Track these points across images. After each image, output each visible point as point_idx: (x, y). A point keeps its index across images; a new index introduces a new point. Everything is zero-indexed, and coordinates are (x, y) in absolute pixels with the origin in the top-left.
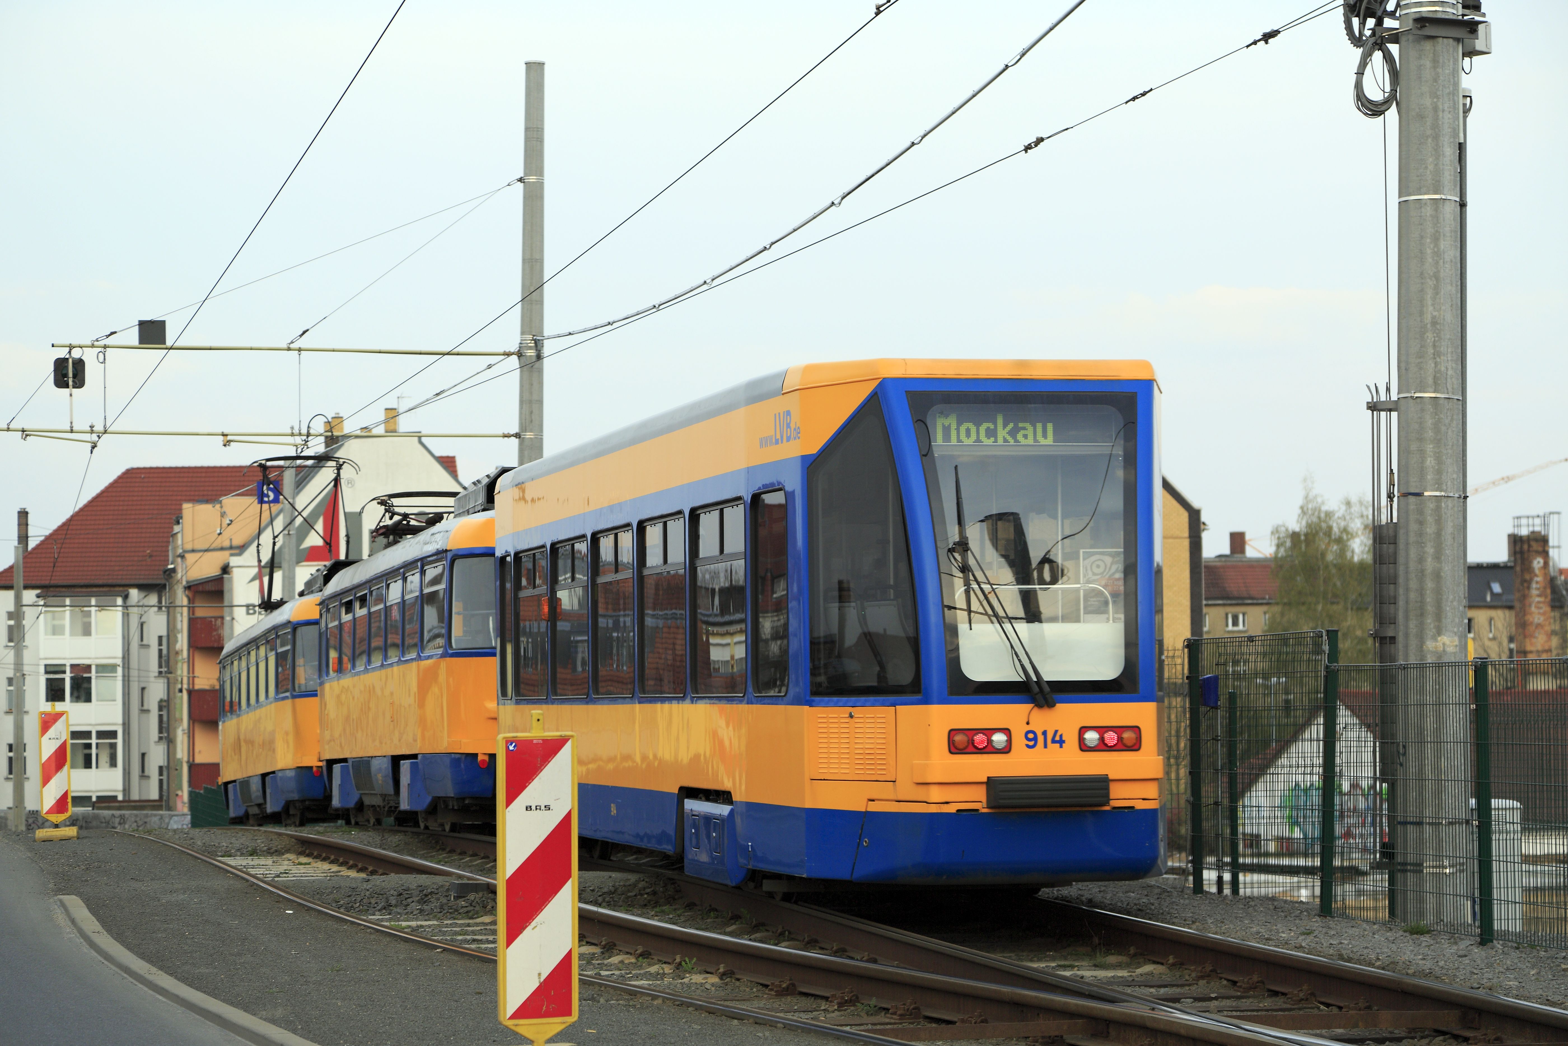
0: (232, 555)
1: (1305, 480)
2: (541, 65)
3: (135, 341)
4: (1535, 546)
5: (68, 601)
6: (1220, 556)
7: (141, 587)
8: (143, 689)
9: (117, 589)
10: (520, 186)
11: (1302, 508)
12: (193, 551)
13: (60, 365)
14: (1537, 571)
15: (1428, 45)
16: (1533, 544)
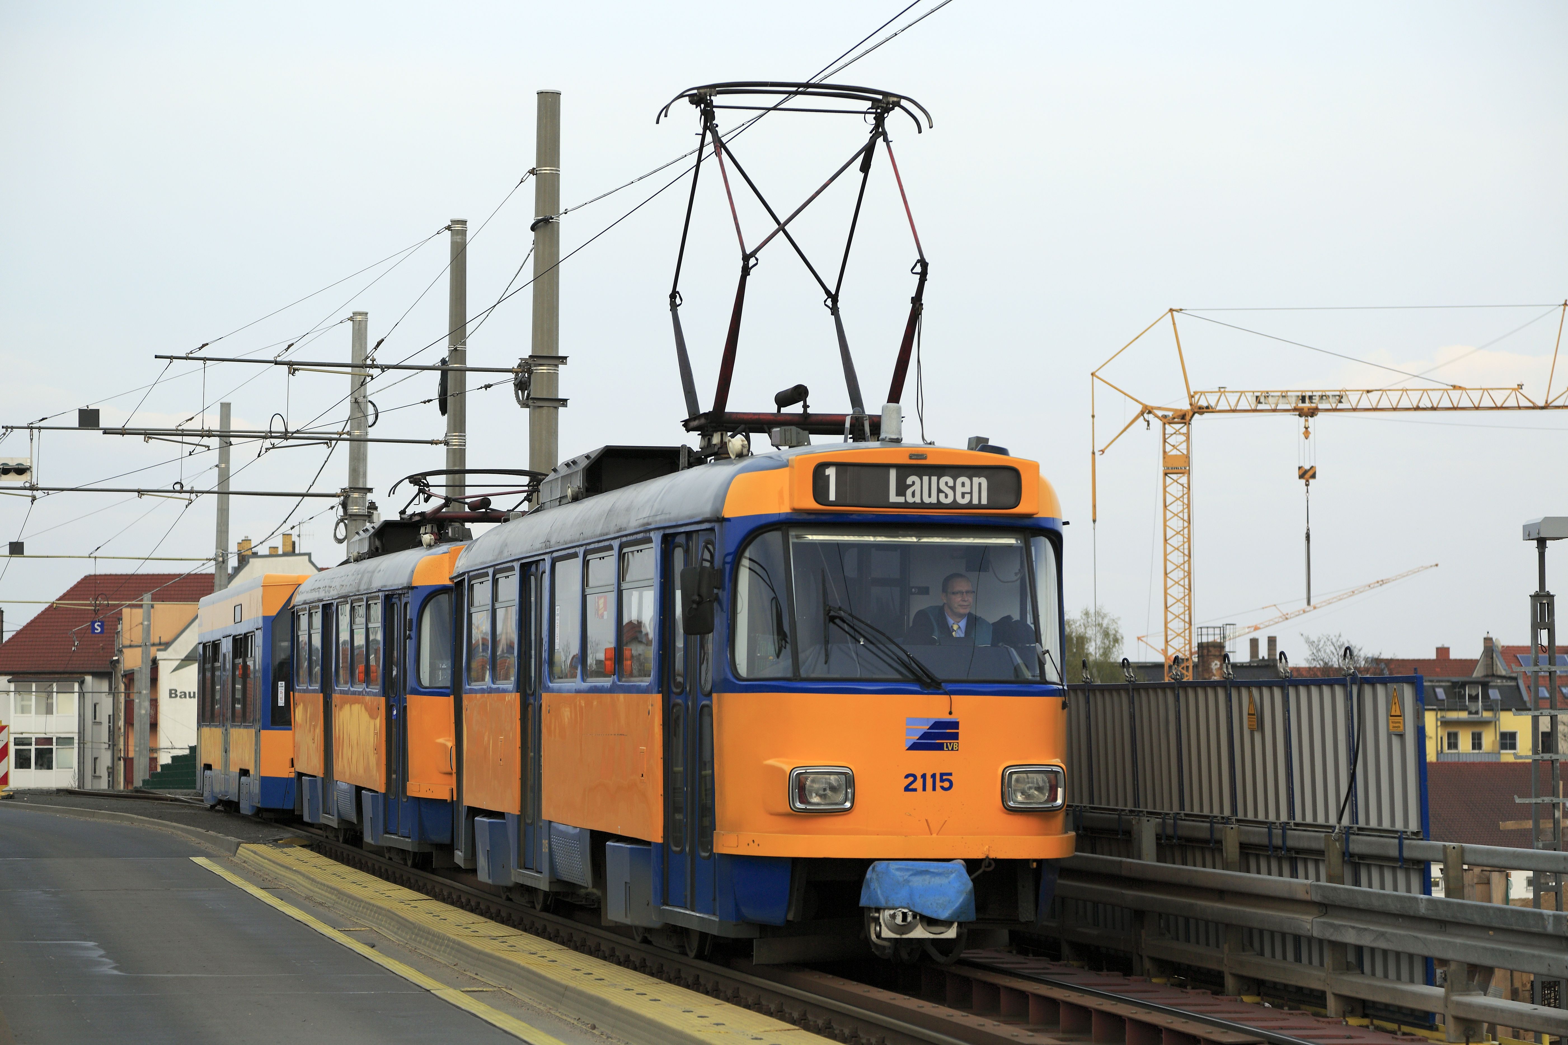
0: (159, 650)
2: (229, 405)
3: (7, 553)
4: (1213, 651)
7: (95, 675)
8: (96, 759)
9: (75, 676)
10: (217, 469)
12: (130, 646)
14: (1214, 672)
15: (354, 522)
16: (1211, 649)
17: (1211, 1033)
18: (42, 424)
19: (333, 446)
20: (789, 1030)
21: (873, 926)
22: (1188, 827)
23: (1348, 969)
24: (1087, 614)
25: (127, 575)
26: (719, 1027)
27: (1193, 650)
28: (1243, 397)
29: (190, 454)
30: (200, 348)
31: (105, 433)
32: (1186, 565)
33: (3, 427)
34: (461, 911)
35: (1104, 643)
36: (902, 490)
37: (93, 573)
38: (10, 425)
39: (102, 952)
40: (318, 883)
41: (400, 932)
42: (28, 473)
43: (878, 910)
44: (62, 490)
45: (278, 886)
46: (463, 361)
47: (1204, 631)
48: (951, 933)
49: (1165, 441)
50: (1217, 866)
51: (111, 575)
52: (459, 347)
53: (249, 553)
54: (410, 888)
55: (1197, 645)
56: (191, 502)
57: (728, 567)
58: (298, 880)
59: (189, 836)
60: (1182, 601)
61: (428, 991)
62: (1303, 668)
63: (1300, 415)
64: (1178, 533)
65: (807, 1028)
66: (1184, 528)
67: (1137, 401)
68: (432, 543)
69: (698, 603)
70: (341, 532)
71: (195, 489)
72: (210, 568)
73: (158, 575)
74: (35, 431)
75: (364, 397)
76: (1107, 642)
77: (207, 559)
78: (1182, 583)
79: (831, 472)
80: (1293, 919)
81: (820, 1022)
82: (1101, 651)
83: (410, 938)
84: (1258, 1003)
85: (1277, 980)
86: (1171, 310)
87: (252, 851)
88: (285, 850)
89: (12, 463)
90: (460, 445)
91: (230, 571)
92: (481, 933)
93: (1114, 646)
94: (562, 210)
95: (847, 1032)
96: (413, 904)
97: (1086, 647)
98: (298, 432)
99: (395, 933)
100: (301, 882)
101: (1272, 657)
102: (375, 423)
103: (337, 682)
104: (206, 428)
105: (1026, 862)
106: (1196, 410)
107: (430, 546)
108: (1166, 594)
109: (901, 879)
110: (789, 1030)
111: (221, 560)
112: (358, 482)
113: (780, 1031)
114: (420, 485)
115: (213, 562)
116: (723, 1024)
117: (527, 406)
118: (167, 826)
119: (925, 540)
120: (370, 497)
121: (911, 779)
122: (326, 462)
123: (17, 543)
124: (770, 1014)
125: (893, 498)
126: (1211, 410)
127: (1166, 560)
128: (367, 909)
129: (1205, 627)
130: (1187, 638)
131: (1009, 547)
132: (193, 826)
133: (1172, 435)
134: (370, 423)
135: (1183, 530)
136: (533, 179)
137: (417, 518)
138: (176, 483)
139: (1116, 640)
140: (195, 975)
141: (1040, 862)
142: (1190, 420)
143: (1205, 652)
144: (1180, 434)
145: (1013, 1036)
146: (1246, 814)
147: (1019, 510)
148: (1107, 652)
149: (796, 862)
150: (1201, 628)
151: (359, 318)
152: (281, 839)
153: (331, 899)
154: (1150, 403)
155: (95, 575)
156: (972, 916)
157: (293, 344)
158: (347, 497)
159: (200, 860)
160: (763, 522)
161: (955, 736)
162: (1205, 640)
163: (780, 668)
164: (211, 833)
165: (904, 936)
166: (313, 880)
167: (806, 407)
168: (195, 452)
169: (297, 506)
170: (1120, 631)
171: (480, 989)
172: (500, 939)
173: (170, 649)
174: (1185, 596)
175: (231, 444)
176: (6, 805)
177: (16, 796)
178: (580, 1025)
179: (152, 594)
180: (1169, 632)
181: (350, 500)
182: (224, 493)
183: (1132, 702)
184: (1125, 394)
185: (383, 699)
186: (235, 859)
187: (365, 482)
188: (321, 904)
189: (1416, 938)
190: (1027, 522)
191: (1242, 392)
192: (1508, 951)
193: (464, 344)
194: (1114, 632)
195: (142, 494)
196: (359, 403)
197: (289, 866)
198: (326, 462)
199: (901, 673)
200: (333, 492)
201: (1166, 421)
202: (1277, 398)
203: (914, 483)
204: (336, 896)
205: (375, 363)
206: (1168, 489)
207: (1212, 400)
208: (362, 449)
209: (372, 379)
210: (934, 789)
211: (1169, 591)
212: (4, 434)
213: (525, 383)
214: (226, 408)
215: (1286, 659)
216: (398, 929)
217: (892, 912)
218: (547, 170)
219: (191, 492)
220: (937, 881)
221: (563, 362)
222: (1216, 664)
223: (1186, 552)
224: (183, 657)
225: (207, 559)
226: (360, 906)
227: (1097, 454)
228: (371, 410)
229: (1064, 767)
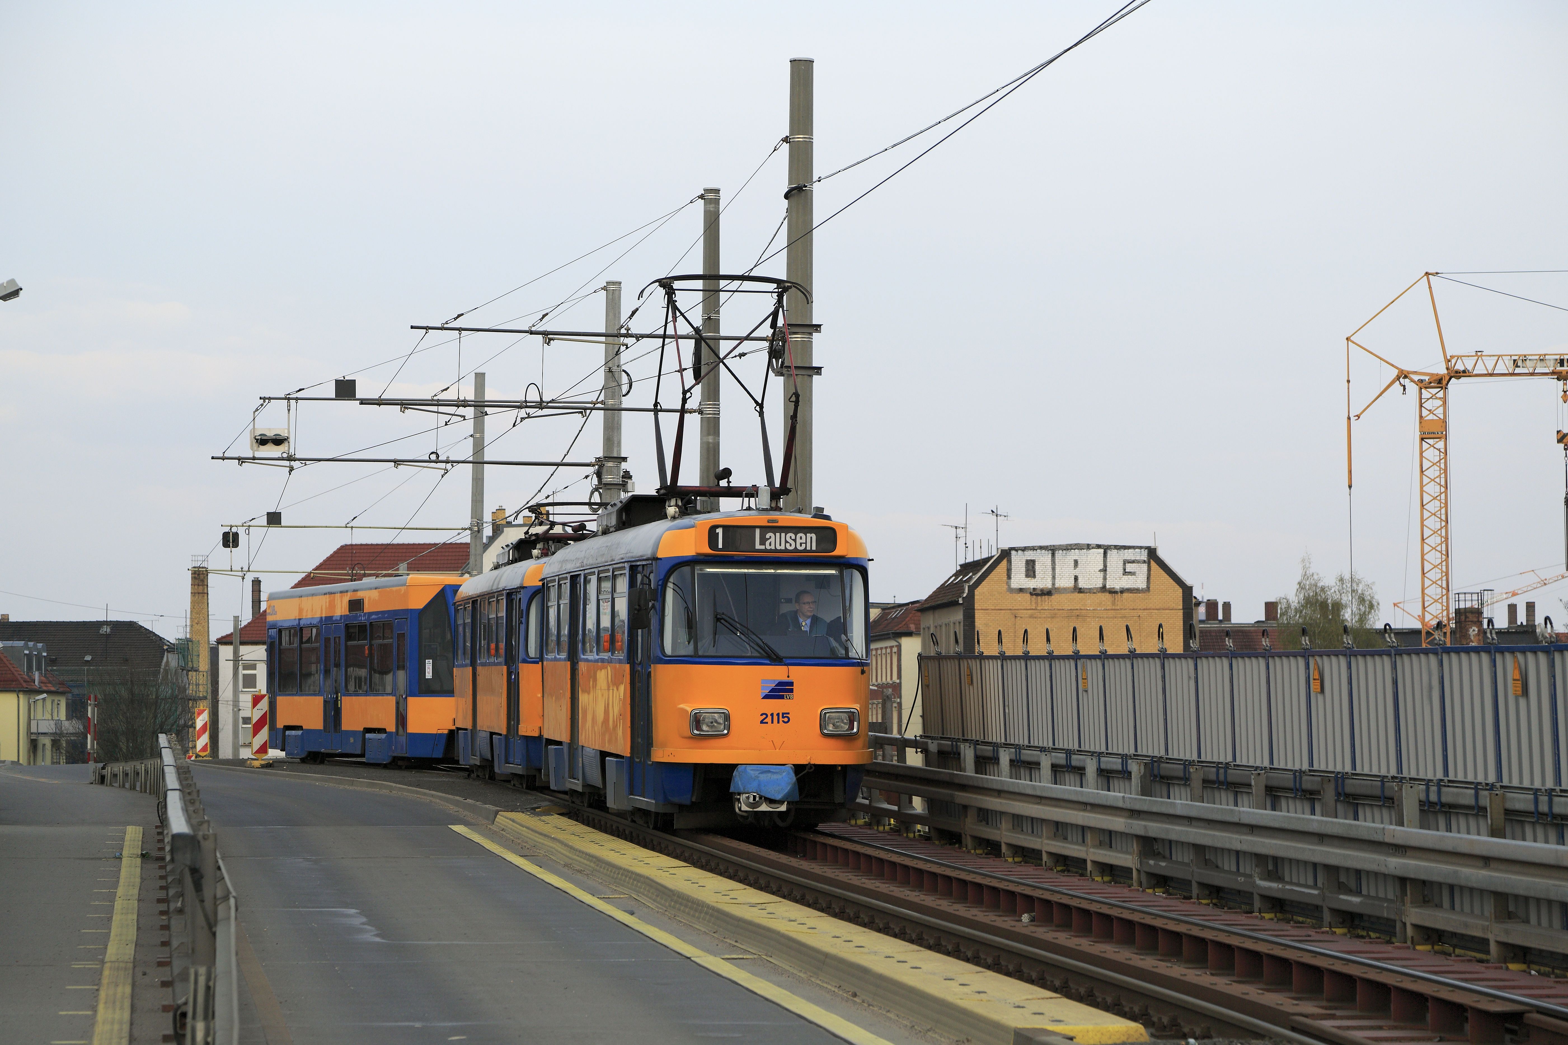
1: (1303, 561)
2: (484, 374)
3: (265, 523)
4: (1471, 617)
6: (1258, 622)
10: (472, 439)
11: (1299, 583)
13: (226, 535)
14: (1472, 638)
15: (609, 491)
16: (1469, 615)
17: (1478, 1001)
18: (299, 395)
19: (587, 415)
20: (1051, 998)
21: (737, 803)
22: (1449, 795)
23: (1510, 918)
24: (1341, 580)
25: (382, 545)
26: (982, 995)
27: (1451, 616)
28: (1500, 361)
29: (446, 424)
30: (455, 319)
31: (361, 403)
32: (1443, 531)
33: (261, 398)
34: (720, 878)
35: (1360, 609)
36: (763, 541)
37: (349, 543)
38: (267, 396)
39: (364, 920)
40: (577, 850)
41: (658, 899)
42: (286, 444)
43: (739, 794)
44: (320, 460)
45: (536, 854)
46: (717, 330)
47: (1462, 597)
48: (783, 808)
49: (1421, 406)
50: (1538, 839)
51: (367, 545)
52: (713, 316)
53: (504, 522)
54: (668, 855)
55: (1454, 611)
56: (447, 471)
57: (660, 587)
58: (556, 848)
59: (447, 804)
60: (1440, 567)
61: (689, 958)
62: (1562, 634)
63: (1558, 379)
64: (1435, 498)
65: (1069, 995)
66: (1441, 493)
67: (1392, 365)
68: (677, 515)
69: (639, 611)
71: (451, 459)
72: (466, 538)
73: (414, 544)
74: (293, 402)
75: (618, 366)
76: (1363, 609)
77: (462, 529)
78: (1439, 548)
79: (720, 531)
80: (1560, 886)
81: (1082, 990)
82: (1357, 617)
83: (670, 906)
84: (1524, 971)
85: (1544, 948)
86: (1427, 274)
87: (510, 819)
88: (543, 818)
89: (270, 434)
90: (715, 414)
91: (485, 540)
92: (740, 900)
93: (1369, 612)
94: (815, 178)
95: (1109, 1000)
96: (672, 871)
97: (1342, 613)
98: (553, 401)
99: (654, 901)
100: (559, 849)
101: (1530, 623)
102: (629, 392)
103: (584, 651)
104: (462, 398)
105: (835, 766)
106: (1452, 375)
107: (538, 558)
108: (1423, 559)
109: (753, 776)
110: (1051, 998)
111: (476, 529)
112: (612, 451)
113: (1043, 999)
114: (536, 514)
116: (985, 992)
117: (782, 374)
118: (425, 794)
119: (779, 571)
120: (624, 466)
121: (764, 716)
122: (580, 431)
123: (274, 513)
124: (1031, 981)
125: (758, 546)
126: (1467, 374)
127: (1422, 525)
128: (626, 876)
129: (1469, 593)
130: (1445, 604)
131: (832, 575)
132: (451, 794)
133: (1428, 399)
134: (624, 392)
135: (1440, 495)
136: (786, 146)
137: (533, 538)
138: (432, 453)
139: (1371, 606)
140: (457, 942)
141: (845, 767)
142: (1447, 384)
143: (1463, 618)
144: (1436, 398)
145: (1278, 1004)
146: (1510, 780)
147: (836, 553)
148: (1363, 618)
149: (696, 766)
150: (1458, 594)
151: (612, 287)
152: (539, 808)
153: (590, 866)
154: (1406, 367)
155: (352, 545)
156: (797, 798)
157: (547, 314)
158: (601, 467)
159: (458, 828)
160: (680, 561)
161: (791, 691)
162: (1462, 606)
163: (689, 650)
164: (469, 801)
165: (755, 810)
166: (571, 848)
167: (729, 482)
168: (450, 422)
169: (552, 475)
170: (1376, 597)
171: (741, 956)
172: (760, 907)
174: (1442, 562)
175: (487, 414)
176: (266, 774)
177: (275, 764)
178: (841, 993)
179: (408, 564)
180: (1426, 598)
181: (604, 470)
182: (478, 462)
183: (1394, 668)
184: (1381, 359)
185: (627, 667)
186: (493, 827)
187: (619, 451)
188: (580, 871)
190: (842, 560)
191: (1499, 356)
193: (718, 312)
194: (1369, 598)
195: (398, 464)
196: (613, 372)
197: (548, 834)
198: (580, 431)
199: (759, 652)
200: (588, 461)
201: (1422, 385)
202: (1535, 361)
203: (770, 537)
204: (595, 863)
205: (630, 332)
206: (1424, 454)
207: (1469, 364)
208: (616, 419)
209: (627, 348)
210: (778, 722)
211: (1426, 557)
212: (262, 405)
213: (779, 352)
214: (480, 378)
215: (1551, 623)
216: (657, 896)
217: (747, 795)
218: (800, 138)
219: (447, 462)
220: (775, 777)
221: (817, 330)
222: (1474, 630)
223: (1443, 517)
225: (462, 529)
226: (618, 874)
227: (1353, 419)
228: (625, 379)
229: (858, 709)
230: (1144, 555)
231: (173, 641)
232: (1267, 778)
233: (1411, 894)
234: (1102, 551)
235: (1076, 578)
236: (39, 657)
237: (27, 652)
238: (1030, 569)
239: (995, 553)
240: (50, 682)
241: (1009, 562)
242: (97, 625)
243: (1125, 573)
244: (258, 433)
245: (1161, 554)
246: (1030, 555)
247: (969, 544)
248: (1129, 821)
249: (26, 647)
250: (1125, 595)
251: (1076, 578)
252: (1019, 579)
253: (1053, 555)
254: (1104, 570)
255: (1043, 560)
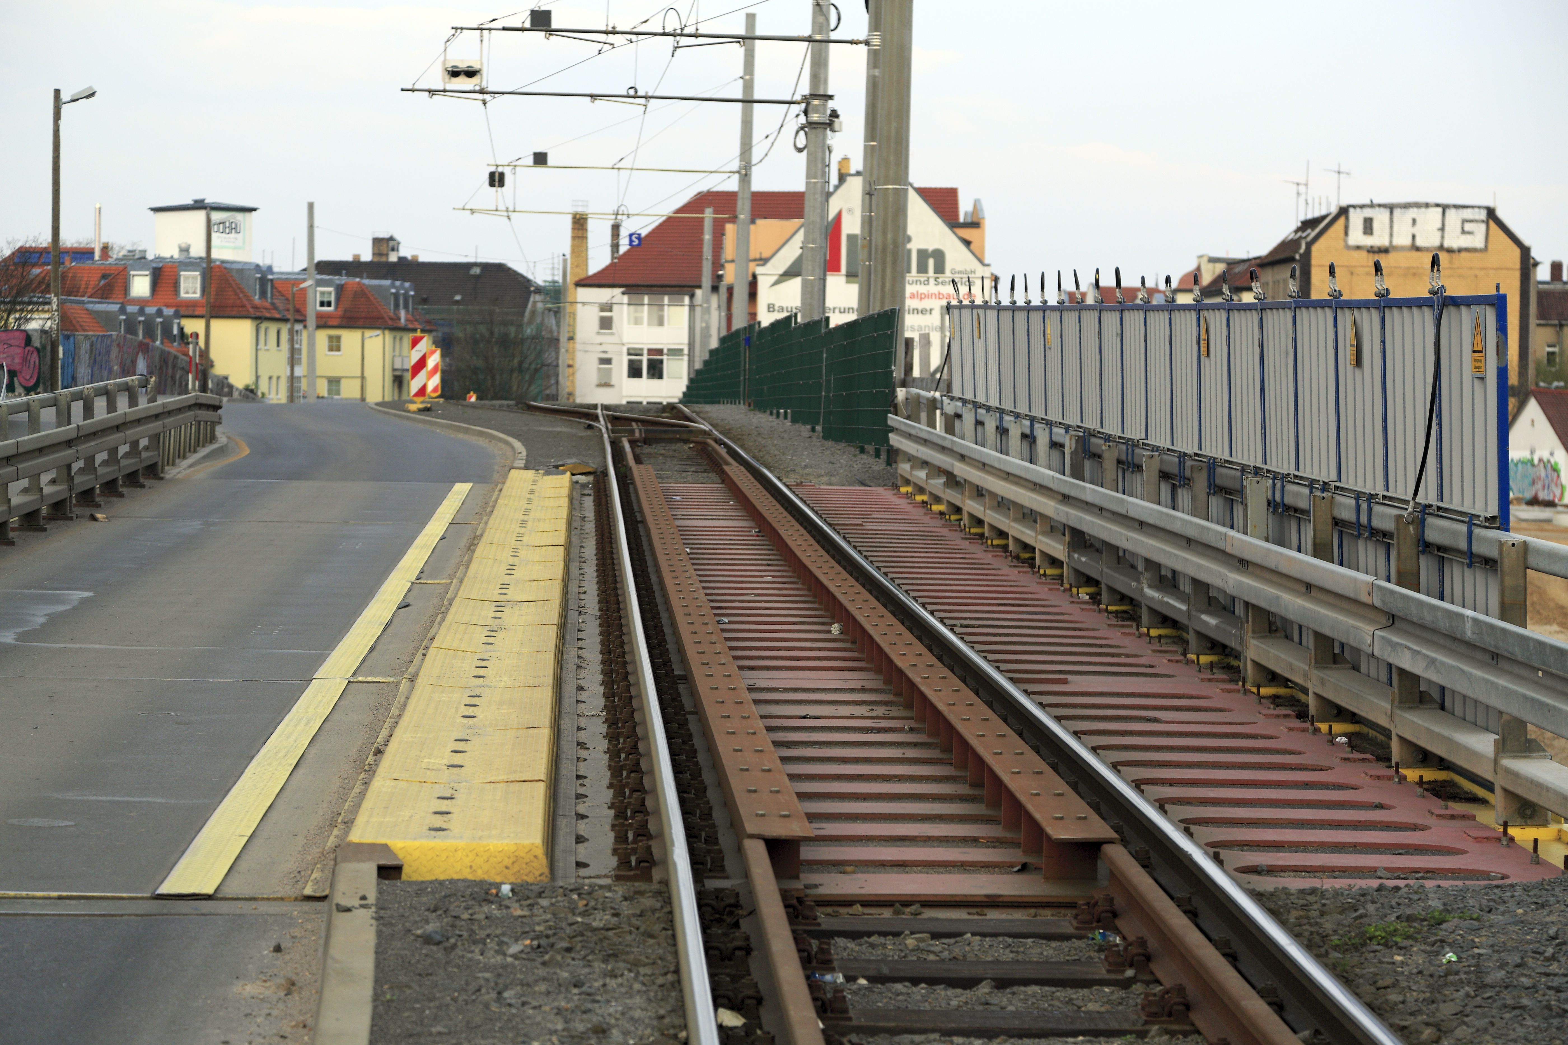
5: (646, 299)
13: (492, 175)
23: (1335, 662)
38: (459, 26)
70: (802, 141)
89: (463, 66)
115: (737, 176)
120: (831, 104)
173: (769, 265)
187: (826, 88)
189: (1462, 671)
192: (1548, 705)
224: (781, 271)
230: (1483, 215)
231: (540, 282)
232: (1162, 461)
233: (1253, 620)
234: (1440, 210)
235: (1414, 237)
236: (406, 297)
237: (393, 291)
238: (1368, 226)
239: (1334, 210)
240: (416, 320)
241: (1347, 219)
242: (466, 267)
243: (1463, 232)
244: (449, 65)
245: (1500, 214)
246: (1368, 213)
247: (1310, 201)
248: (1058, 506)
249: (393, 286)
250: (1463, 254)
251: (1414, 237)
252: (1357, 237)
253: (1391, 213)
254: (1442, 229)
255: (1381, 218)
